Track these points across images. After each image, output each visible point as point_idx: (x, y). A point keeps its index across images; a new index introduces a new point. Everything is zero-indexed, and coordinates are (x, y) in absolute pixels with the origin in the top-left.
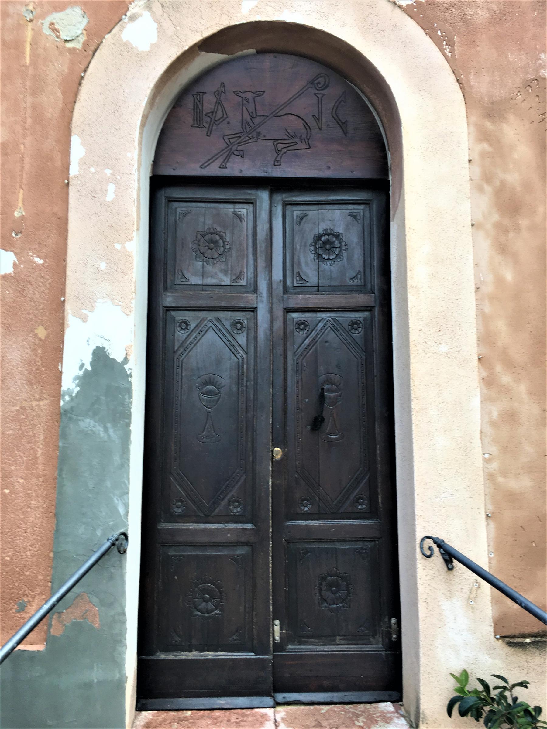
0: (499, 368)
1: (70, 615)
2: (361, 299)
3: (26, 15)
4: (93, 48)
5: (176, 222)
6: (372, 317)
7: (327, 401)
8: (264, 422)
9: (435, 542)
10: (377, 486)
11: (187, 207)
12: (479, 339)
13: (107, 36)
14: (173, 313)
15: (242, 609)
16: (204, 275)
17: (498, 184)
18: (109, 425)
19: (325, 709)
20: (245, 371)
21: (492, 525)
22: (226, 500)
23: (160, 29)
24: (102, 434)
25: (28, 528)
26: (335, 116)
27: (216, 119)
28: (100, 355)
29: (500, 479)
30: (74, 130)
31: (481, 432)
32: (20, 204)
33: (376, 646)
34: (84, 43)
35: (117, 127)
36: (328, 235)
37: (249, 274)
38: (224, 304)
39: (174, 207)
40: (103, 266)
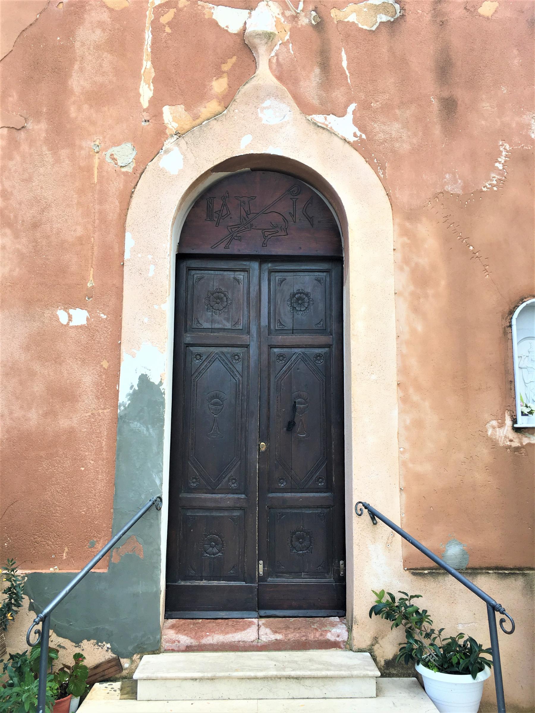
0: (411, 391)
1: (123, 550)
2: (323, 339)
3: (94, 148)
4: (140, 172)
5: (193, 284)
6: (331, 352)
7: (298, 410)
8: (254, 425)
9: (363, 505)
10: (332, 470)
11: (201, 274)
12: (398, 371)
13: (149, 164)
14: (191, 348)
15: (237, 553)
16: (213, 321)
17: (413, 265)
18: (149, 426)
19: (292, 619)
20: (241, 389)
21: (404, 495)
22: (227, 479)
23: (185, 159)
24: (145, 432)
25: (96, 493)
26: (305, 214)
27: (223, 215)
28: (144, 380)
29: (410, 465)
30: (127, 228)
31: (398, 433)
32: (91, 278)
33: (329, 580)
34: (133, 168)
35: (156, 227)
36: (301, 293)
37: (244, 321)
38: (226, 342)
39: (192, 274)
40: (146, 320)
